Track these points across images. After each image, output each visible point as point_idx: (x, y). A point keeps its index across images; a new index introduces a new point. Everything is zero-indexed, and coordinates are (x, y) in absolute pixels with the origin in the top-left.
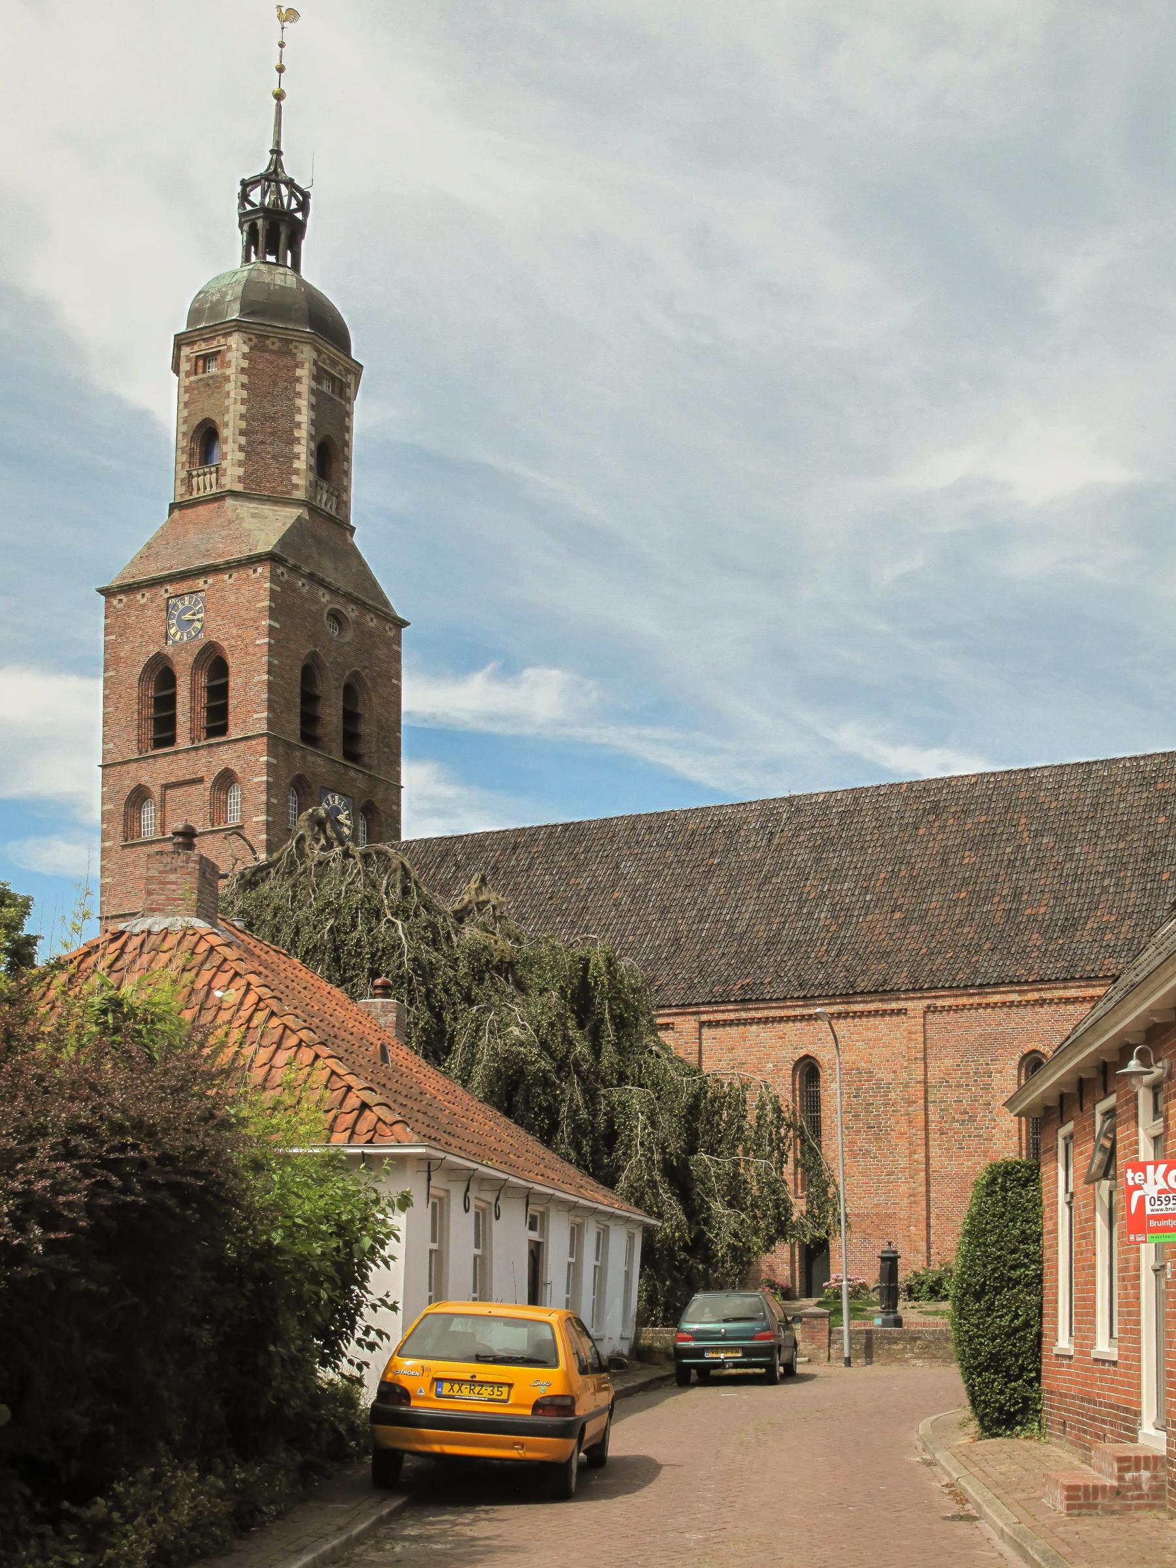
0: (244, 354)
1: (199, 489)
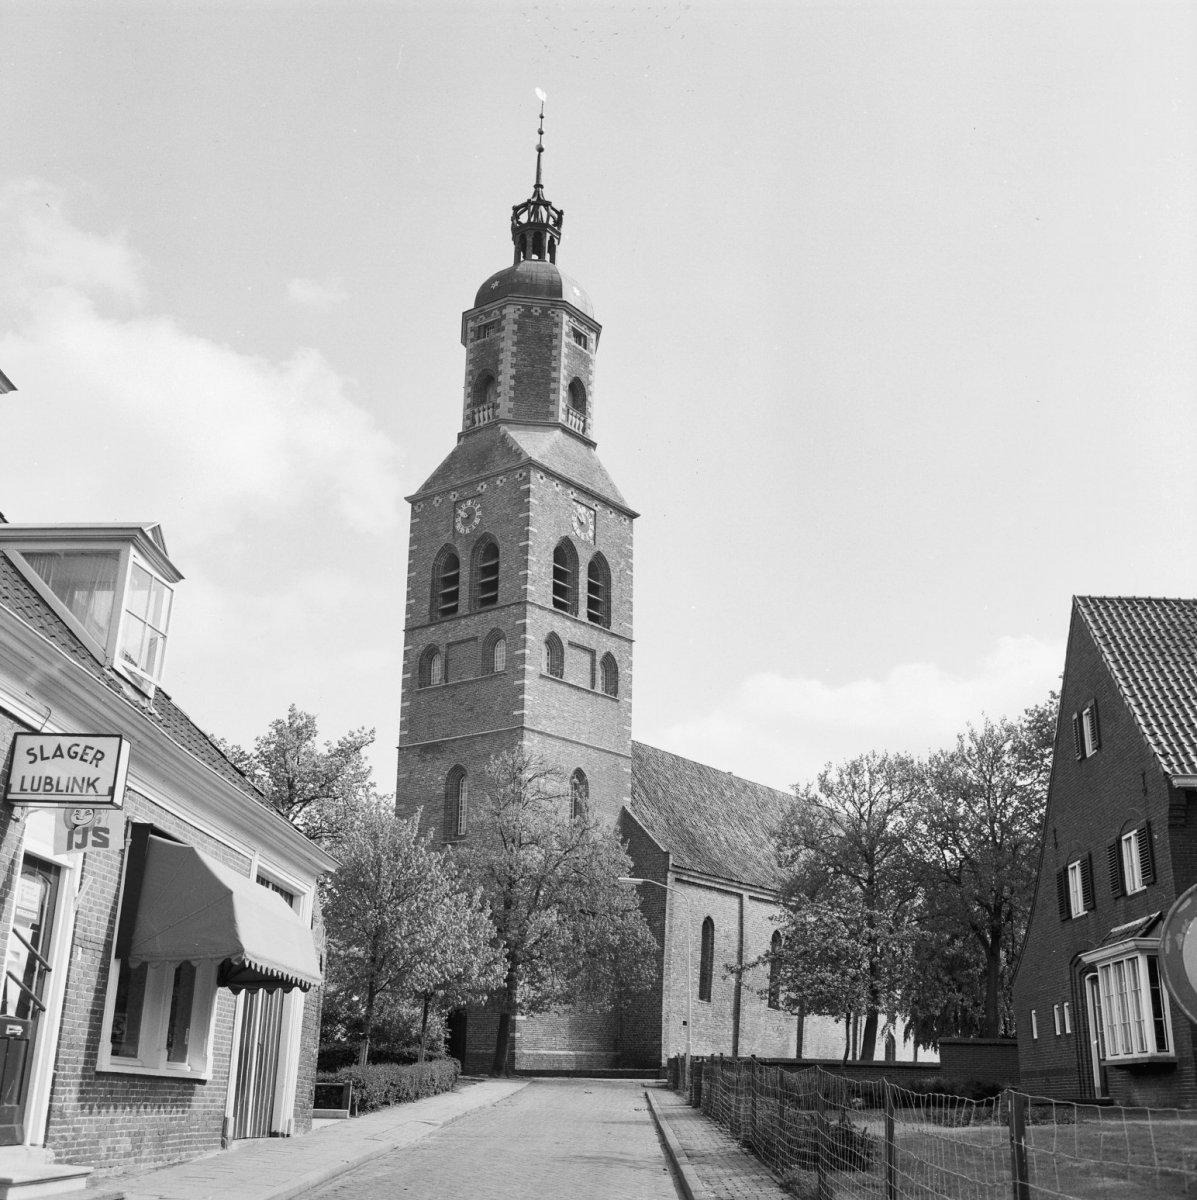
0: (512, 353)
1: (480, 421)
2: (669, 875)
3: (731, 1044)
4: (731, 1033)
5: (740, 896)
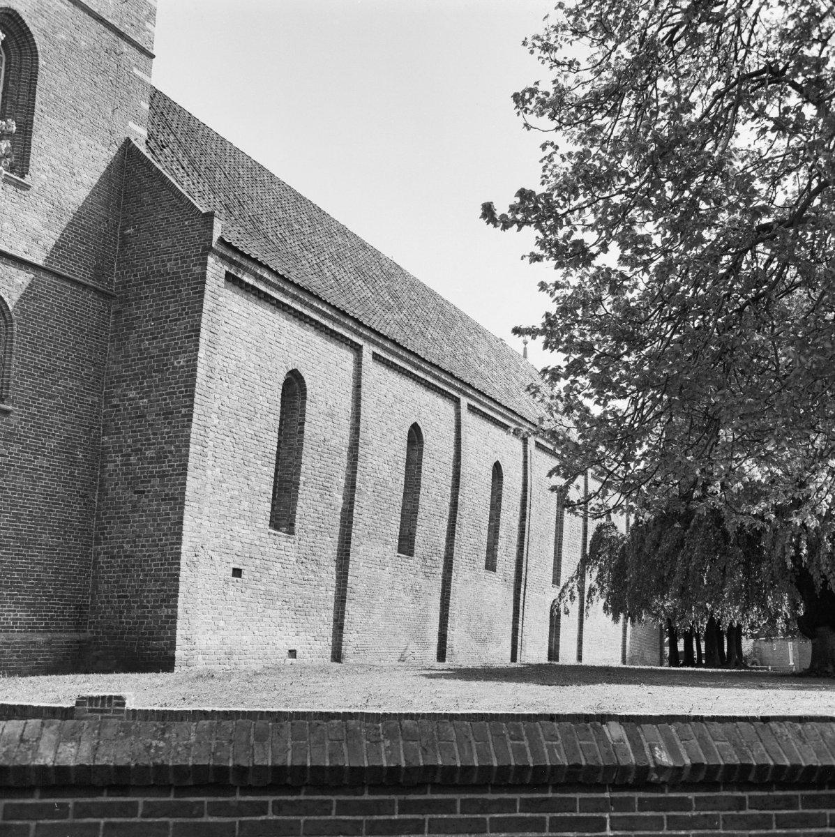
2: (211, 260)
3: (331, 613)
4: (332, 594)
5: (357, 349)
